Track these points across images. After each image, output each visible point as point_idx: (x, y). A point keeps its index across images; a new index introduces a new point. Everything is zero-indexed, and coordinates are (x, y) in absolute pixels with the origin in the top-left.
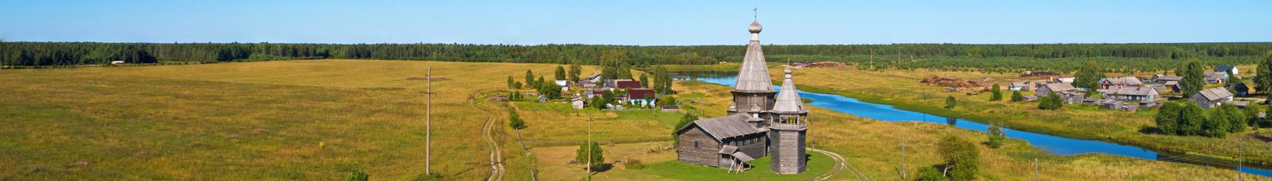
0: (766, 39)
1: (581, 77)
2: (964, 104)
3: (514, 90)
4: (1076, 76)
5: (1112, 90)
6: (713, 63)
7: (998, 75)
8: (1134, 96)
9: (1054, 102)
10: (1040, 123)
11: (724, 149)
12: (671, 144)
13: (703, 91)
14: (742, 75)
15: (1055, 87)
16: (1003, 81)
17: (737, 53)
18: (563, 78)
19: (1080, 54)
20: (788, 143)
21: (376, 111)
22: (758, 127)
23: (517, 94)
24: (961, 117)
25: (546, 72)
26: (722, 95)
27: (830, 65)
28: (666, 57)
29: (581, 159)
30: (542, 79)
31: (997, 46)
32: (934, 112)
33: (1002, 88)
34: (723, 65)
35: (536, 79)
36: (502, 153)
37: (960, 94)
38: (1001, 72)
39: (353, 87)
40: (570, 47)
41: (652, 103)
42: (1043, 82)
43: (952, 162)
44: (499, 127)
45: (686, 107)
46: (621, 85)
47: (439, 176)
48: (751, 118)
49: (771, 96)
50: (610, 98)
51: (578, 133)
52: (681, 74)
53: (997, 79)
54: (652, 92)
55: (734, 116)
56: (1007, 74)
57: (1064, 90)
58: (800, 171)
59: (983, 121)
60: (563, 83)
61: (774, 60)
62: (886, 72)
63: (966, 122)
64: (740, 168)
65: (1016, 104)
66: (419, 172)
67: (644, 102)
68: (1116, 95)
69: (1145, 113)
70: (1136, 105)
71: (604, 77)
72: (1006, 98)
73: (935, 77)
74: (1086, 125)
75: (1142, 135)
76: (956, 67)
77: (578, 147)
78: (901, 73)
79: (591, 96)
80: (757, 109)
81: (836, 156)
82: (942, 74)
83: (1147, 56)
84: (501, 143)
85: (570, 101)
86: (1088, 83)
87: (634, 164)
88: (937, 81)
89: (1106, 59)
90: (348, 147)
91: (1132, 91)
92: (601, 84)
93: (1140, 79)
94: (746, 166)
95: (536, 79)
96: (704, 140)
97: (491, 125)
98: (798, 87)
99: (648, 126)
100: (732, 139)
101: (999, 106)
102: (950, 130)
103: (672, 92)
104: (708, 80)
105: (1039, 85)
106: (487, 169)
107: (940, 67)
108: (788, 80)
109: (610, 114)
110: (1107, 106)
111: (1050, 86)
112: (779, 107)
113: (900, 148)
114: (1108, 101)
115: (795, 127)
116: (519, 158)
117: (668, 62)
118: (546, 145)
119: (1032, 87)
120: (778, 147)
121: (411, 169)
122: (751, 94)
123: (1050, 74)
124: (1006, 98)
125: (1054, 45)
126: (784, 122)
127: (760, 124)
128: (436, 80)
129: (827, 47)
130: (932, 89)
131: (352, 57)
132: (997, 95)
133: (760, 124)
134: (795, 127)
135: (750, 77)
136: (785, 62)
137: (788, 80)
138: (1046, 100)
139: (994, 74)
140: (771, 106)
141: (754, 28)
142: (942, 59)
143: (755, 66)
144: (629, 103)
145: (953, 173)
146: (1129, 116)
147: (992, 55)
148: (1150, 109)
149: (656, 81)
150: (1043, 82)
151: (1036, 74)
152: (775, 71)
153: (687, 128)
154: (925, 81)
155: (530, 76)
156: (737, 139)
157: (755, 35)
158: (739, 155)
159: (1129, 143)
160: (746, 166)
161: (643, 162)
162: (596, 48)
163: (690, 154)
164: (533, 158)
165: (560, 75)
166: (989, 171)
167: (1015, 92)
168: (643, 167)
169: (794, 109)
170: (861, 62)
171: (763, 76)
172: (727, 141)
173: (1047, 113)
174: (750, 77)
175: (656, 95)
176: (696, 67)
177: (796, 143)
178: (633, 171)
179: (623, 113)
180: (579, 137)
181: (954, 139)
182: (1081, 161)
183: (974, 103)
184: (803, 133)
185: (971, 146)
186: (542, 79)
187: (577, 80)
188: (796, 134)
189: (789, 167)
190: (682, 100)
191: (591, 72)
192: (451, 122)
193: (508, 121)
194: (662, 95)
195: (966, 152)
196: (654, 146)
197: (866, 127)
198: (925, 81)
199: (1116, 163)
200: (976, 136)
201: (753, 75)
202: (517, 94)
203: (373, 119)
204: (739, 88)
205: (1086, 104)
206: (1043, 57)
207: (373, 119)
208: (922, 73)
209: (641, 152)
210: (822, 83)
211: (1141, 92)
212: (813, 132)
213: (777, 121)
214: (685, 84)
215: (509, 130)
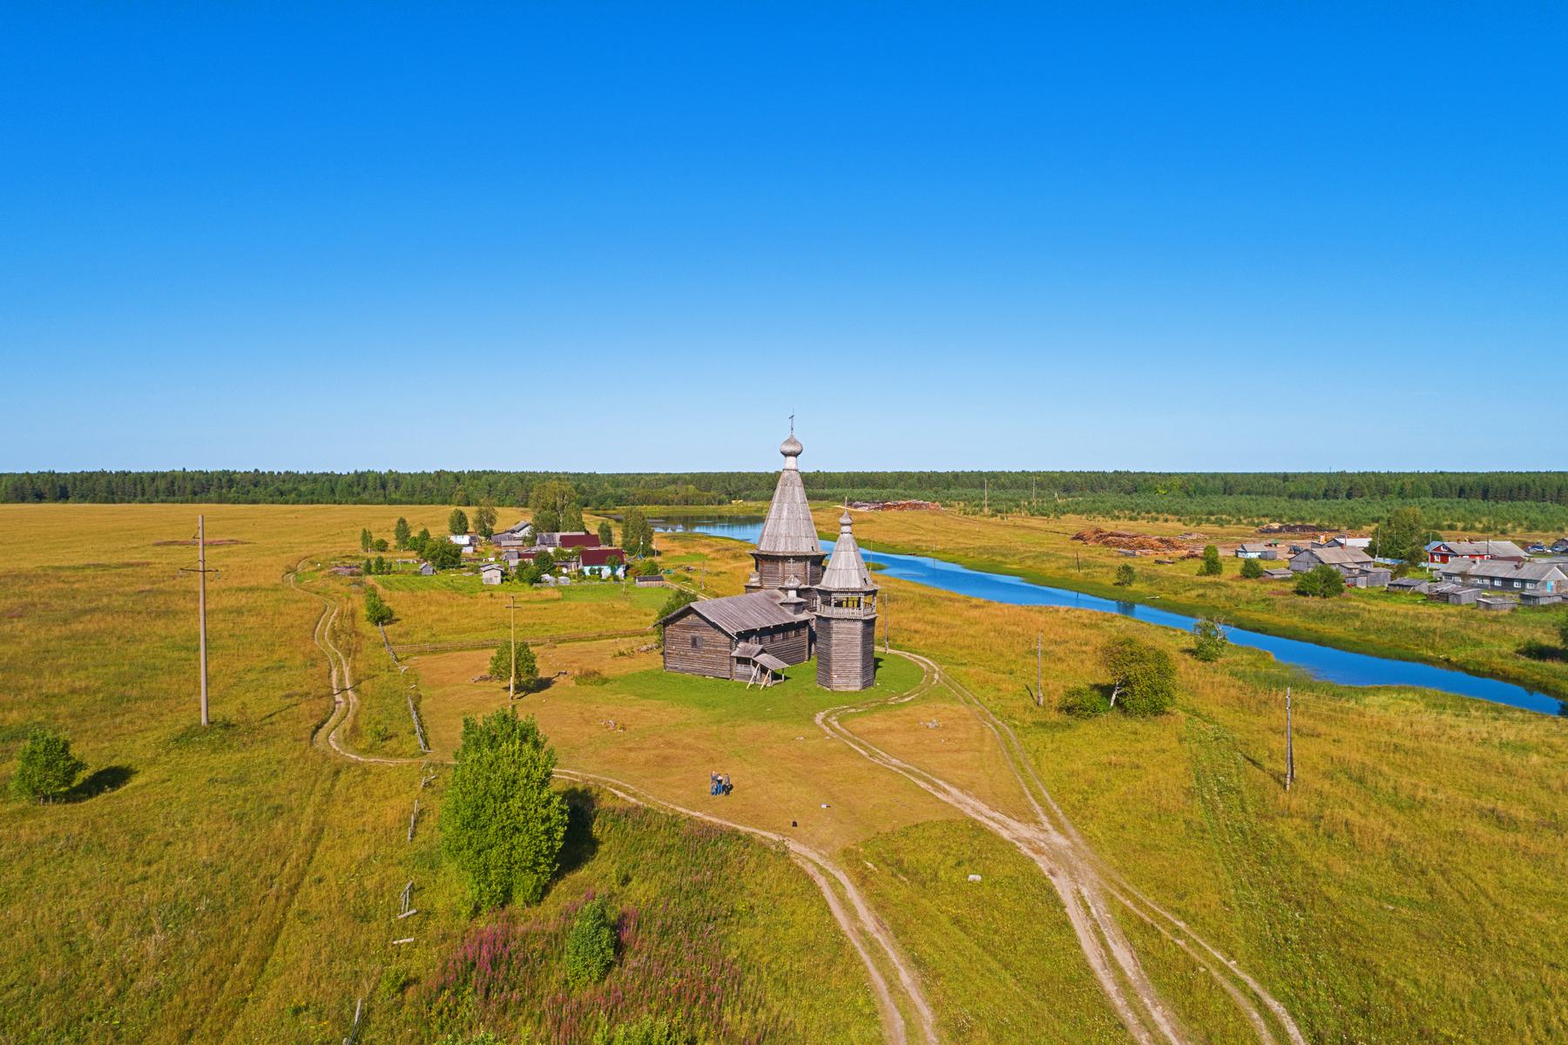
0: (810, 464)
1: (496, 528)
2: (1150, 578)
3: (373, 555)
4: (1375, 534)
5: (1453, 565)
6: (720, 503)
7: (1216, 529)
8: (1507, 582)
9: (1328, 582)
10: (1295, 620)
11: (741, 649)
12: (652, 640)
13: (707, 551)
14: (770, 523)
15: (1328, 556)
16: (1225, 542)
17: (765, 485)
18: (466, 532)
19: (1385, 492)
20: (845, 639)
21: (85, 612)
22: (796, 612)
23: (380, 561)
24: (1142, 603)
25: (433, 520)
26: (736, 557)
27: (915, 507)
28: (640, 492)
29: (499, 673)
30: (425, 534)
31: (1214, 476)
32: (1096, 591)
33: (1221, 553)
34: (737, 506)
35: (414, 534)
36: (353, 669)
37: (1142, 562)
38: (1220, 523)
39: (27, 565)
40: (475, 475)
41: (620, 572)
42: (1305, 544)
43: (1126, 683)
44: (347, 623)
45: (676, 578)
46: (566, 541)
47: (227, 726)
48: (784, 599)
49: (818, 562)
50: (548, 564)
51: (493, 626)
52: (668, 520)
53: (1212, 535)
54: (619, 553)
55: (756, 594)
56: (1233, 528)
57: (1348, 561)
58: (865, 686)
59: (1188, 611)
60: (465, 540)
61: (823, 498)
62: (1009, 520)
64: (766, 680)
65: (1250, 584)
66: (185, 722)
67: (606, 571)
68: (1463, 575)
69: (1536, 616)
70: (1511, 599)
71: (536, 529)
72: (1231, 571)
73: (1098, 531)
74: (1394, 630)
75: (1523, 660)
76: (1135, 513)
77: (493, 653)
78: (1036, 522)
79: (514, 562)
80: (796, 583)
81: (925, 662)
82: (1108, 525)
83: (1543, 498)
84: (349, 653)
85: (477, 570)
86: (1401, 548)
87: (590, 677)
88: (1102, 537)
89: (1444, 502)
90: (20, 690)
91: (1504, 570)
92: (531, 541)
93: (1524, 546)
94: (776, 676)
95: (414, 534)
96: (707, 634)
97: (330, 621)
98: (860, 543)
99: (615, 612)
100: (753, 632)
101: (1216, 584)
102: (1122, 622)
103: (653, 553)
104: (711, 531)
105: (1296, 551)
106: (324, 703)
107: (1107, 513)
108: (846, 535)
109: (548, 592)
110: (1444, 597)
111: (1317, 551)
112: (830, 581)
113: (1034, 653)
114: (1445, 587)
115: (858, 613)
116: (385, 676)
117: (646, 501)
118: (435, 651)
119: (1282, 551)
120: (829, 645)
121: (168, 719)
122: (785, 559)
123: (1320, 529)
124: (1231, 571)
125: (1328, 476)
126: (839, 604)
127: (799, 607)
128: (219, 544)
129: (911, 475)
130: (1094, 552)
131: (23, 500)
132: (1213, 566)
133: (799, 607)
134: (858, 613)
135: (783, 530)
136: (841, 501)
137: (846, 535)
138: (1311, 578)
139: (1207, 527)
140: (816, 578)
141: (789, 449)
142: (1111, 499)
143: (791, 511)
144: (581, 572)
145: (1127, 701)
146: (1495, 620)
147: (1203, 492)
148: (1546, 608)
149: (625, 535)
150: (1305, 544)
151: (1290, 529)
152: (824, 516)
153: (677, 614)
154: (1078, 537)
155: (402, 530)
156: (765, 632)
157: (791, 459)
158: (764, 659)
159: (1492, 674)
160: (776, 676)
161: (605, 674)
162: (521, 477)
163: (684, 657)
164: (411, 676)
165: (460, 526)
166: (1195, 702)
167: (1248, 562)
168: (605, 681)
169: (856, 584)
170: (968, 500)
171: (804, 528)
172: (745, 636)
173: (1313, 602)
174: (783, 530)
175: (626, 558)
176: (693, 510)
177: (859, 640)
178: (588, 689)
179: (569, 589)
180: (495, 634)
181: (1130, 642)
182: (1382, 699)
183: (1168, 578)
184: (869, 623)
185: (1161, 657)
186: (425, 534)
187: (488, 534)
188: (859, 625)
189: (848, 679)
190: (668, 566)
191: (514, 520)
192: (252, 621)
193: (363, 612)
194: (635, 556)
195: (1152, 666)
196: (624, 645)
197: (976, 613)
198: (1078, 537)
199: (1462, 710)
200: (1172, 639)
201: (787, 525)
202: (380, 561)
203: (78, 627)
204: (765, 548)
205: (1394, 590)
206: (1306, 497)
207: (78, 627)
208: (1073, 523)
209: (601, 655)
210: (902, 539)
211: (1526, 572)
212: (886, 619)
213: (827, 603)
214: (674, 538)
215: (366, 627)
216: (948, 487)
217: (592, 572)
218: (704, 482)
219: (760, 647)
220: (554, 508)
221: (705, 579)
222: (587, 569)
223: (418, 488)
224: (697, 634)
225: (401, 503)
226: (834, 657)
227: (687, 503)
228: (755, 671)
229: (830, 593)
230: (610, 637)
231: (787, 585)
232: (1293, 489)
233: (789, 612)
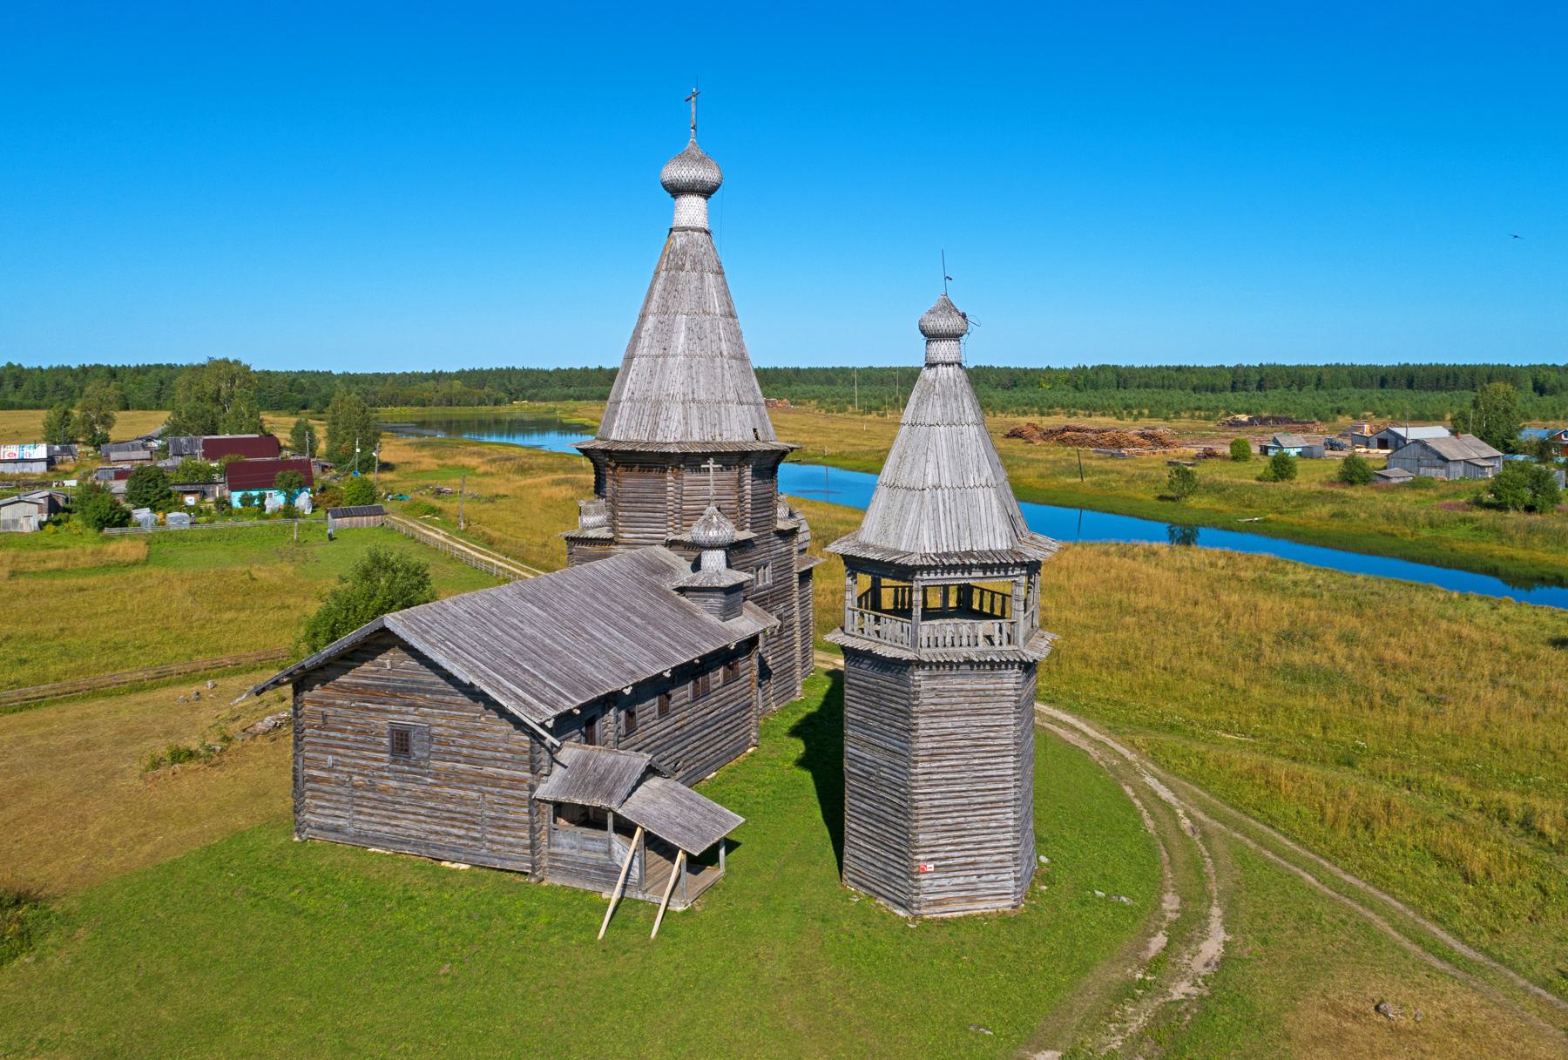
1: (114, 434)
6: (497, 402)
13: (473, 462)
41: (303, 500)
63: (1214, 532)
64: (671, 891)
67: (276, 500)
80: (726, 531)
122: (691, 460)
135: (676, 381)
143: (696, 334)
144: (223, 504)
149: (332, 436)
151: (1264, 421)
172: (579, 722)
216: (790, 384)
217: (246, 501)
218: (475, 379)
219: (642, 760)
220: (216, 399)
221: (467, 507)
222: (236, 498)
223: (50, 388)
224: (410, 718)
225: (21, 407)
226: (925, 797)
227: (450, 403)
228: (625, 852)
229: (905, 572)
230: (189, 677)
231: (697, 533)
232: (1196, 382)
233: (707, 612)
